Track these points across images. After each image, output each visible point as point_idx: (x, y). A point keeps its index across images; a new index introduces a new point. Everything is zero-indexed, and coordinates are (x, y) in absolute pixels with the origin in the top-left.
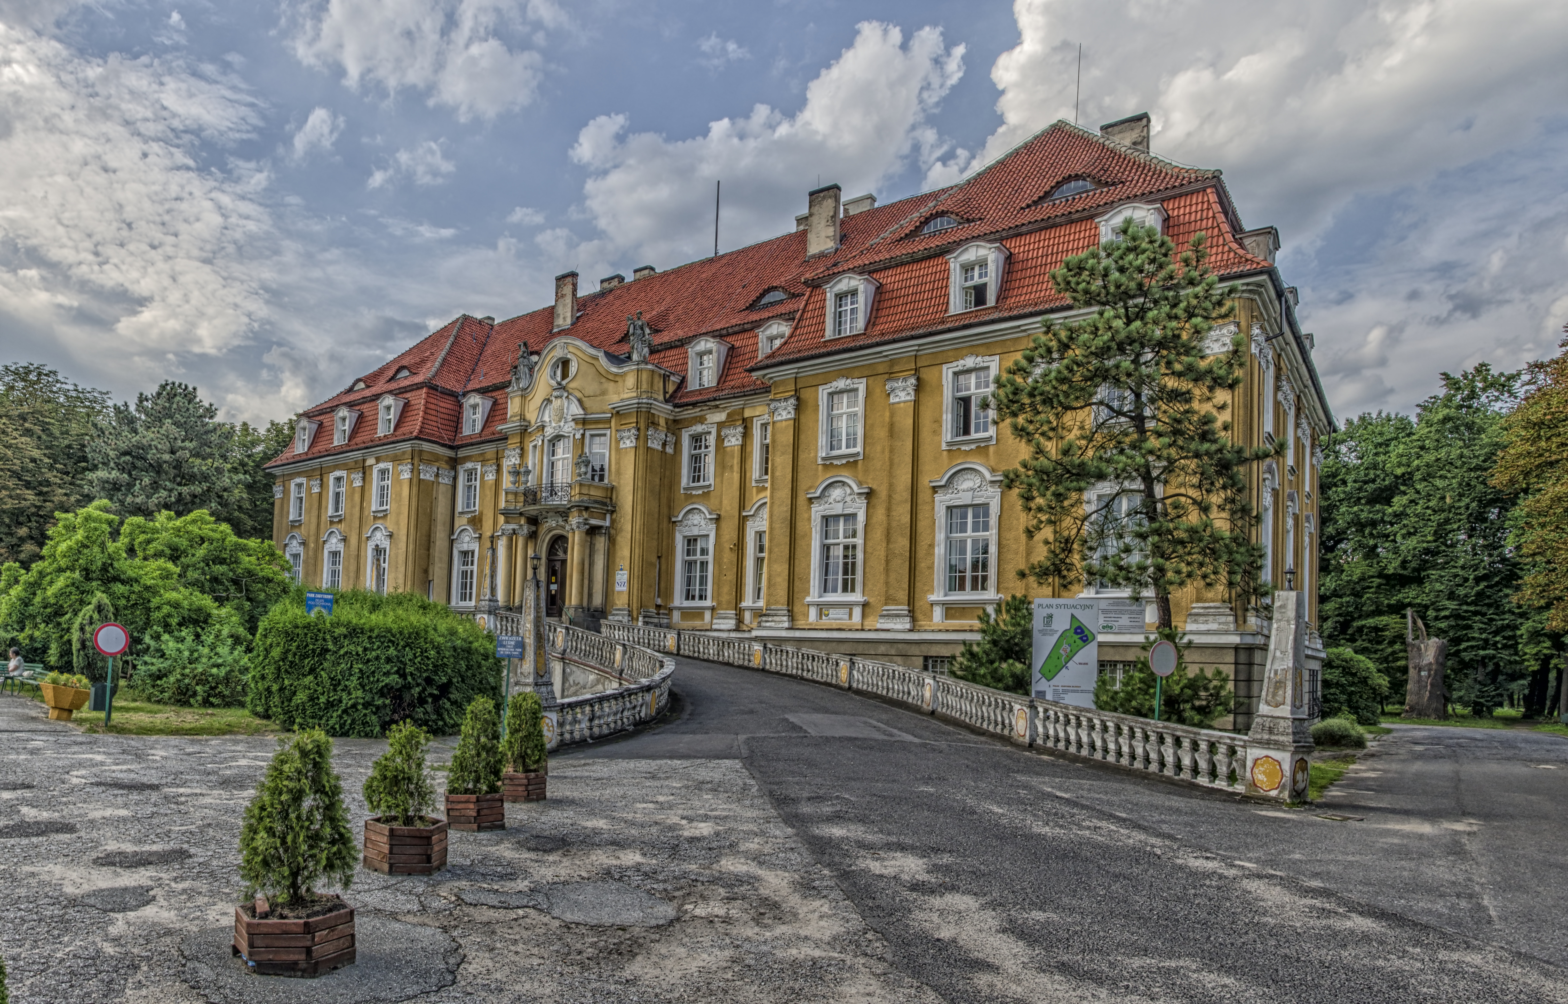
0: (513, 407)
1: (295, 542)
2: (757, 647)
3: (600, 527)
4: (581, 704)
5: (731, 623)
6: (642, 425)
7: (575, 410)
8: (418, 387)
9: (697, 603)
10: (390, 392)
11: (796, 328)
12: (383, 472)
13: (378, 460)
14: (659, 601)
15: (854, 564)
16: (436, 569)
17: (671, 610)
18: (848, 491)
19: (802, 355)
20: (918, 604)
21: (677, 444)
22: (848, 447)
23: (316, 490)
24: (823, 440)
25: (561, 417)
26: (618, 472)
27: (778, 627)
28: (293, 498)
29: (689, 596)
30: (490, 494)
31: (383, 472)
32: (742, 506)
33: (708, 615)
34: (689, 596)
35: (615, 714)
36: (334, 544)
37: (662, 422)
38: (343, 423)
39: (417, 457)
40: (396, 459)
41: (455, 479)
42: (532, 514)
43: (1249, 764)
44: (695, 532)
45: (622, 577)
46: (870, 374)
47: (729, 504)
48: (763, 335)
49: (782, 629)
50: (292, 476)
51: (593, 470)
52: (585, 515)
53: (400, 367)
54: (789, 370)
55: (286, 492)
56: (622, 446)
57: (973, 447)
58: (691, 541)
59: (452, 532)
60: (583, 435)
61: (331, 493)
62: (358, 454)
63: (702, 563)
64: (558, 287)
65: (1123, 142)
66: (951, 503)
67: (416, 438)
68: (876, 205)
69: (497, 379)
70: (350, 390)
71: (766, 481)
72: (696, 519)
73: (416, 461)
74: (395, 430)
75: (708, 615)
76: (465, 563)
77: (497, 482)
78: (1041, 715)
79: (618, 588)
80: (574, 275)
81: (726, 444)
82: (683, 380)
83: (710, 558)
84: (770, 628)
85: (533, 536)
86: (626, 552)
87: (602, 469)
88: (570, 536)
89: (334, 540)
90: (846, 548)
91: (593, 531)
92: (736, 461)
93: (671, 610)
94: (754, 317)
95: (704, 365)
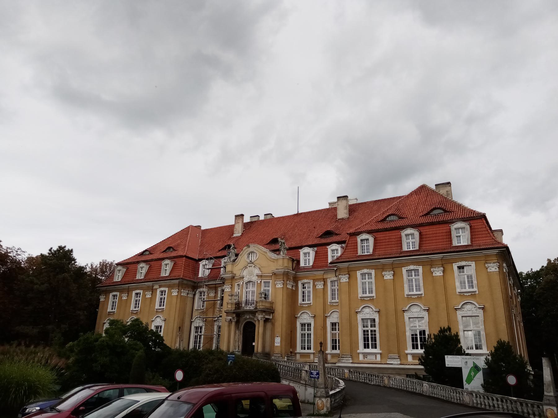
3: (269, 319)
6: (285, 280)
7: (257, 271)
8: (181, 256)
9: (306, 351)
12: (162, 292)
13: (160, 287)
17: (296, 354)
18: (371, 310)
21: (297, 286)
22: (369, 293)
24: (360, 290)
25: (251, 274)
27: (347, 363)
29: (366, 346)
31: (162, 292)
32: (324, 312)
33: (312, 356)
38: (142, 270)
40: (170, 287)
41: (194, 295)
42: (238, 313)
43: (545, 410)
44: (305, 321)
45: (278, 341)
46: (376, 268)
47: (319, 312)
48: (330, 248)
49: (349, 363)
54: (346, 265)
55: (107, 299)
56: (277, 287)
57: (470, 294)
61: (133, 300)
62: (150, 284)
63: (308, 334)
65: (443, 191)
66: (410, 316)
67: (182, 279)
72: (305, 316)
75: (312, 356)
78: (474, 396)
79: (276, 345)
80: (242, 215)
81: (317, 287)
83: (312, 332)
84: (344, 363)
85: (237, 323)
90: (371, 331)
91: (266, 321)
92: (321, 295)
93: (296, 354)
94: (323, 241)
95: (307, 257)
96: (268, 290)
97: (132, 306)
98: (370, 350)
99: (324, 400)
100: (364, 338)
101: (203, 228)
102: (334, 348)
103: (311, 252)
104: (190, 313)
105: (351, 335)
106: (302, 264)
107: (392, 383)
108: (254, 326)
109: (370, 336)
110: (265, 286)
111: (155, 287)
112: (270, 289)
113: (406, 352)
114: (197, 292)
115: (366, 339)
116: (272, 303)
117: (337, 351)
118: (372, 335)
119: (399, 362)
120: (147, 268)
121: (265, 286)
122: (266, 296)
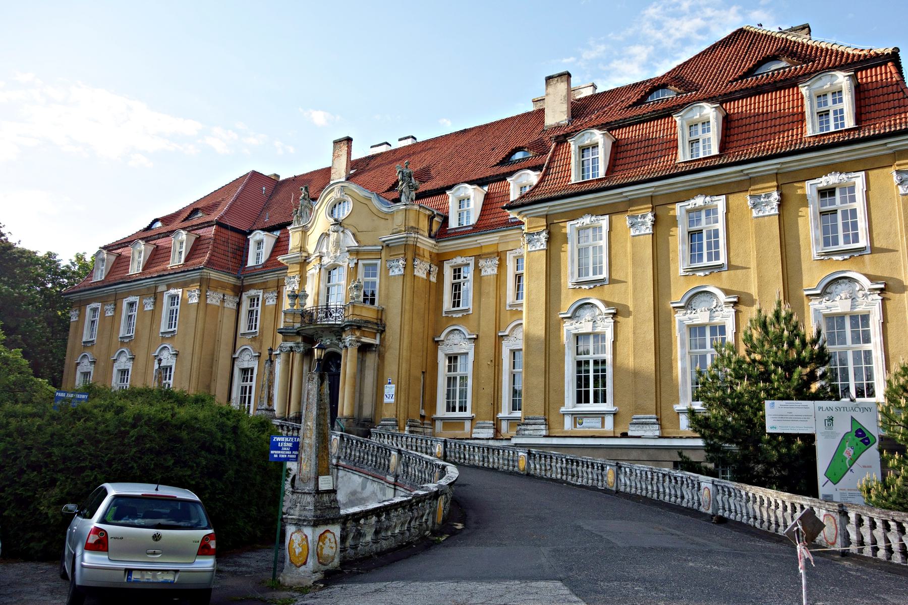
0: (294, 240)
1: (86, 362)
2: (522, 454)
3: (371, 345)
4: (366, 514)
5: (490, 433)
9: (457, 414)
10: (184, 229)
11: (545, 175)
13: (169, 287)
14: (423, 413)
15: (604, 377)
16: (218, 385)
17: (434, 421)
19: (553, 195)
20: (664, 413)
21: (440, 275)
23: (149, 308)
26: (388, 297)
27: (536, 437)
28: (87, 325)
29: (582, 397)
30: (270, 318)
32: (498, 327)
33: (468, 424)
34: (451, 408)
35: (403, 524)
36: (123, 362)
37: (427, 255)
38: (139, 255)
39: (205, 285)
40: (184, 285)
41: (239, 304)
45: (390, 390)
50: (88, 302)
51: (365, 295)
52: (358, 333)
53: (194, 210)
55: (82, 316)
56: (391, 274)
58: (453, 358)
59: (234, 352)
60: (357, 264)
64: (334, 147)
68: (597, 91)
69: (278, 220)
70: (149, 228)
71: (521, 305)
72: (456, 338)
73: (204, 289)
74: (187, 260)
75: (468, 424)
76: (245, 380)
77: (278, 306)
79: (386, 400)
80: (349, 140)
81: (483, 273)
82: (446, 219)
84: (530, 436)
85: (308, 353)
86: (394, 368)
87: (373, 294)
88: (343, 353)
89: (123, 359)
90: (596, 362)
91: (364, 349)
93: (434, 421)
94: (505, 169)
96: (374, 283)
97: (122, 328)
98: (591, 407)
99: (308, 531)
100: (579, 379)
101: (281, 179)
102: (515, 407)
103: (475, 195)
104: (231, 341)
105: (547, 372)
106: (453, 224)
107: (626, 483)
108: (339, 356)
109: (591, 374)
110: (367, 275)
111: (160, 289)
112: (377, 280)
113: (677, 407)
114: (244, 296)
115: (582, 381)
116: (381, 311)
117: (518, 414)
118: (596, 371)
119: (657, 433)
120: (149, 253)
121: (367, 275)
122: (370, 299)
